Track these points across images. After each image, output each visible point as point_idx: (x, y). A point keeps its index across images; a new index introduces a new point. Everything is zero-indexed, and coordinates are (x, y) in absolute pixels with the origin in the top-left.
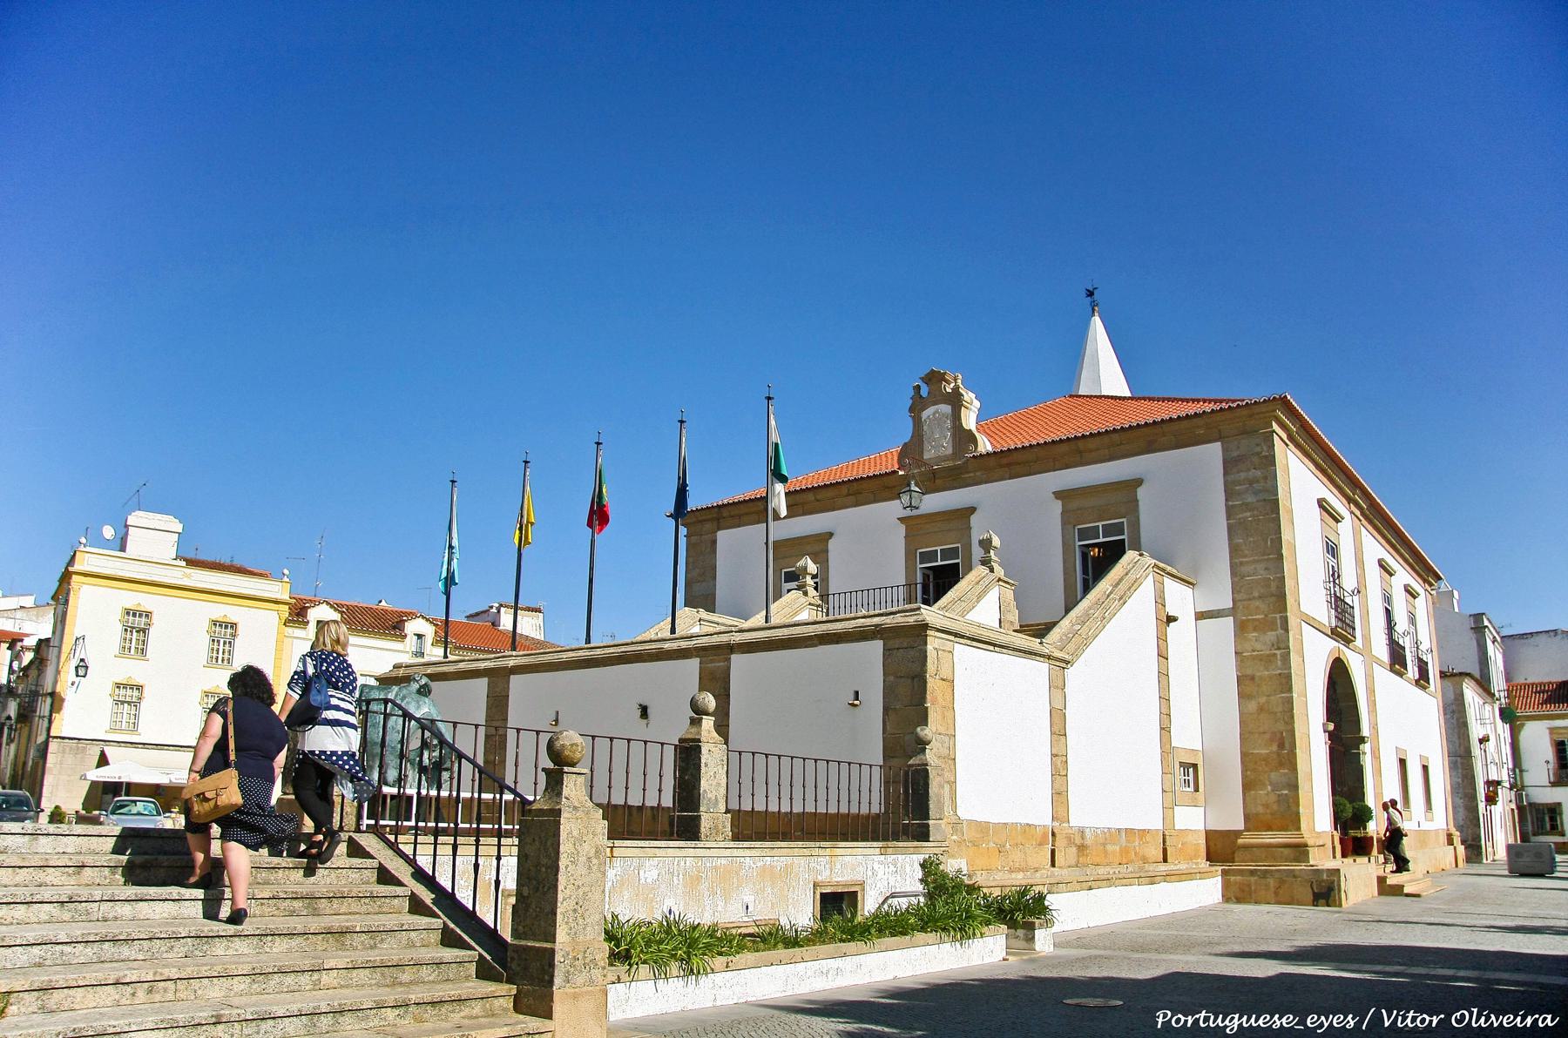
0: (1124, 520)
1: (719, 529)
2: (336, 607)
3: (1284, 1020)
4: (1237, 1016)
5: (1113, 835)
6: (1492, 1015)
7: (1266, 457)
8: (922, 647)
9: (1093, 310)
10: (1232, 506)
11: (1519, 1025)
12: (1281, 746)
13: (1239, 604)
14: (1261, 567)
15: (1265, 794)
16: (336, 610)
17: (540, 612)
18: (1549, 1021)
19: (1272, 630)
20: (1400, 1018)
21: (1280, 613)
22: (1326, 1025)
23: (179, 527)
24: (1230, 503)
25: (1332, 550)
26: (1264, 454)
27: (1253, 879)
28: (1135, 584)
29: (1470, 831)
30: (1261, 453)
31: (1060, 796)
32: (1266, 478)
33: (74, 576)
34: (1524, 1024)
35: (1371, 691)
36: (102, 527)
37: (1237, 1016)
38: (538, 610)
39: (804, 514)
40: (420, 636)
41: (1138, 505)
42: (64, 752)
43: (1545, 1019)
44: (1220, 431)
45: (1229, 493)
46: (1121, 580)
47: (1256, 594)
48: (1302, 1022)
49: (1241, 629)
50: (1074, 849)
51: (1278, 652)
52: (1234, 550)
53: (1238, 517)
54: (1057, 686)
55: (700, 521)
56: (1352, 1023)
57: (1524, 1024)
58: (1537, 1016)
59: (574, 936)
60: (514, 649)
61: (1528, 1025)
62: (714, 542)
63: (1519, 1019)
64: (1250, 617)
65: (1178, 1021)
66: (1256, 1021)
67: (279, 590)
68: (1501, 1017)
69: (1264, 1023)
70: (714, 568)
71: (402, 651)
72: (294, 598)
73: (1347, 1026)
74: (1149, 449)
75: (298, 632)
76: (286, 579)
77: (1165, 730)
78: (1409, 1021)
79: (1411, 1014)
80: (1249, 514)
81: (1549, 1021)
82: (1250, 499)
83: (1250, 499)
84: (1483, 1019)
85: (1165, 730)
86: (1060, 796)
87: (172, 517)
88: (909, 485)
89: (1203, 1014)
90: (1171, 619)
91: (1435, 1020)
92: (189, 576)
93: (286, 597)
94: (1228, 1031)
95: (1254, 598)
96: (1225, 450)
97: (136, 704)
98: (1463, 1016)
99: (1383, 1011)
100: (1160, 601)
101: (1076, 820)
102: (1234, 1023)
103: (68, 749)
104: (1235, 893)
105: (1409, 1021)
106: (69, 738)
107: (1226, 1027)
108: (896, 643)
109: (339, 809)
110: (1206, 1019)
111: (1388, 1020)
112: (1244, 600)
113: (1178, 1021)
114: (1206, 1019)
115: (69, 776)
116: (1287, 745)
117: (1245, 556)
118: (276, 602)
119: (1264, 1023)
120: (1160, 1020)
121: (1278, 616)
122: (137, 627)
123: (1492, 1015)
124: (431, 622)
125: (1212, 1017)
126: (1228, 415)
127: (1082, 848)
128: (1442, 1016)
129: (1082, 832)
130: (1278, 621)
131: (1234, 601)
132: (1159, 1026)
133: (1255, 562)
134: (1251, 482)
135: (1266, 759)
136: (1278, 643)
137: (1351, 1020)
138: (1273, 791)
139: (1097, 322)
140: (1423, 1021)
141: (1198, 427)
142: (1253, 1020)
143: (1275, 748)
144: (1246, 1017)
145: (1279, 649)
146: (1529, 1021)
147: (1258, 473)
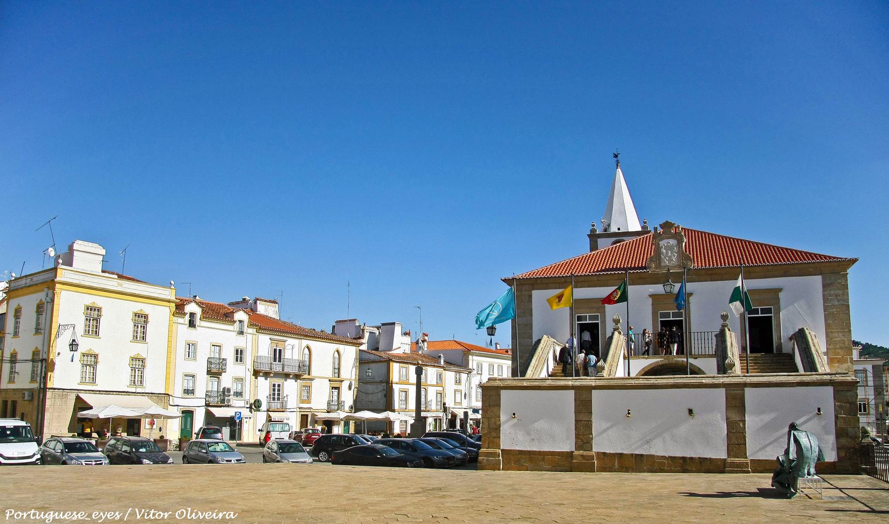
0: (772, 307)
1: (534, 289)
2: (199, 304)
3: (79, 515)
4: (52, 513)
6: (199, 512)
7: (843, 285)
8: (855, 391)
9: (617, 165)
11: (215, 518)
14: (840, 334)
16: (199, 306)
17: (277, 303)
18: (232, 515)
19: (845, 363)
20: (146, 514)
21: (850, 356)
22: (103, 518)
23: (103, 252)
24: (826, 304)
32: (843, 294)
34: (217, 517)
36: (588, 331)
37: (52, 513)
38: (275, 302)
39: (589, 287)
41: (779, 301)
43: (230, 514)
44: (821, 271)
45: (825, 300)
48: (90, 516)
52: (827, 326)
55: (522, 284)
56: (118, 517)
57: (217, 517)
58: (225, 513)
61: (220, 518)
62: (530, 296)
63: (215, 514)
65: (18, 515)
66: (44, 516)
67: (169, 294)
68: (204, 513)
69: (68, 517)
71: (232, 331)
72: (179, 299)
73: (116, 519)
74: (785, 274)
75: (181, 320)
78: (151, 515)
79: (152, 511)
80: (835, 310)
81: (232, 515)
82: (836, 303)
83: (836, 303)
84: (194, 514)
87: (98, 245)
88: (668, 281)
89: (33, 511)
91: (166, 515)
92: (121, 285)
93: (173, 298)
94: (47, 521)
95: (837, 348)
96: (823, 280)
98: (182, 513)
99: (137, 510)
102: (50, 516)
105: (151, 515)
107: (46, 519)
108: (841, 388)
110: (34, 515)
111: (202, 516)
113: (18, 515)
114: (34, 515)
118: (169, 301)
119: (68, 517)
120: (8, 515)
122: (93, 316)
123: (199, 512)
124: (247, 313)
125: (38, 513)
126: (827, 264)
128: (171, 513)
130: (849, 359)
132: (7, 518)
133: (837, 332)
134: (836, 296)
136: (848, 369)
137: (118, 515)
139: (619, 172)
140: (159, 515)
142: (61, 515)
144: (57, 513)
146: (220, 515)
147: (840, 292)
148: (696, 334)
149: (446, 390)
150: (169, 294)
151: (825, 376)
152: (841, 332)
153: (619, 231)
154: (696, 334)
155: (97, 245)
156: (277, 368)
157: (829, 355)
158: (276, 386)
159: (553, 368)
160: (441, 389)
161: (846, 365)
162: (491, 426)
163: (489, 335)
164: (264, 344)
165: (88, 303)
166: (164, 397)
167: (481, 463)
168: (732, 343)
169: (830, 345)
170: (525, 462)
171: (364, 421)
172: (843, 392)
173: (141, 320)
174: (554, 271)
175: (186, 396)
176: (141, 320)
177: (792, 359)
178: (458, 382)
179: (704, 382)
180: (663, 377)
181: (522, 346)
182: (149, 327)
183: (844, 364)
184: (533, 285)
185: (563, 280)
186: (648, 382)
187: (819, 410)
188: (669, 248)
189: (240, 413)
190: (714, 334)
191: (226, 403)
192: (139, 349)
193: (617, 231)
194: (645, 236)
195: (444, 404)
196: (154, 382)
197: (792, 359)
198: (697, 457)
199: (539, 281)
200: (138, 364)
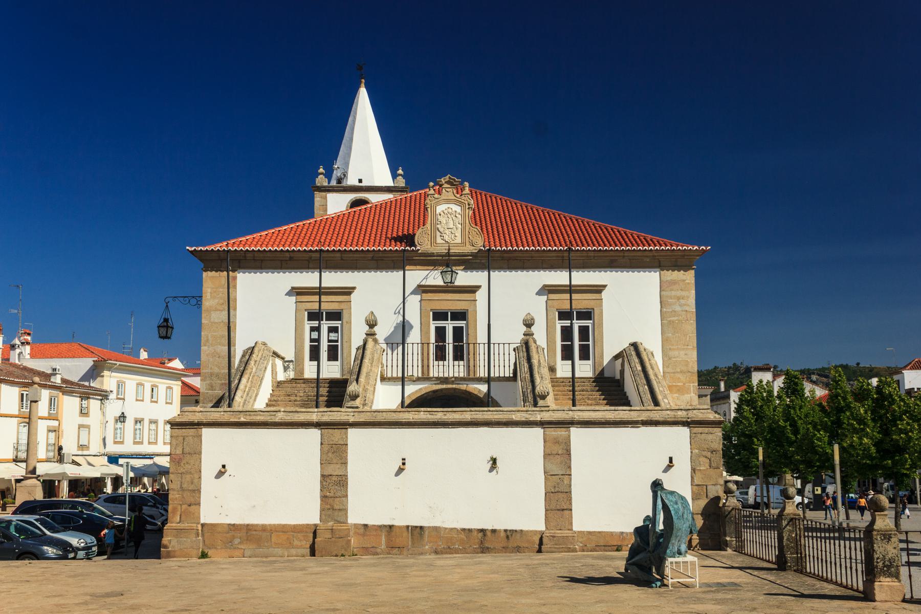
10: (666, 311)
13: (667, 375)
19: (687, 393)
26: (687, 281)
30: (685, 280)
47: (679, 370)
53: (669, 319)
60: (317, 407)
64: (674, 384)
109: (825, 572)
112: (671, 373)
115: (739, 604)
117: (673, 345)
121: (692, 385)
130: (692, 389)
136: (691, 402)
139: (363, 97)
141: (647, 257)
148: (496, 346)
149: (64, 427)
151: (680, 413)
153: (360, 184)
154: (496, 346)
158: (24, 407)
159: (271, 392)
160: (55, 423)
161: (689, 395)
162: (185, 486)
163: (161, 337)
167: (166, 547)
168: (539, 361)
169: (668, 367)
170: (240, 543)
171: (86, 479)
172: (703, 435)
174: (320, 233)
177: (619, 386)
178: (84, 413)
179: (514, 417)
180: (455, 409)
181: (219, 357)
183: (686, 395)
184: (239, 262)
185: (287, 255)
186: (432, 417)
187: (494, 461)
188: (447, 214)
190: (512, 346)
193: (357, 184)
194: (424, 191)
195: (60, 448)
197: (619, 386)
198: (619, 531)
199: (249, 255)
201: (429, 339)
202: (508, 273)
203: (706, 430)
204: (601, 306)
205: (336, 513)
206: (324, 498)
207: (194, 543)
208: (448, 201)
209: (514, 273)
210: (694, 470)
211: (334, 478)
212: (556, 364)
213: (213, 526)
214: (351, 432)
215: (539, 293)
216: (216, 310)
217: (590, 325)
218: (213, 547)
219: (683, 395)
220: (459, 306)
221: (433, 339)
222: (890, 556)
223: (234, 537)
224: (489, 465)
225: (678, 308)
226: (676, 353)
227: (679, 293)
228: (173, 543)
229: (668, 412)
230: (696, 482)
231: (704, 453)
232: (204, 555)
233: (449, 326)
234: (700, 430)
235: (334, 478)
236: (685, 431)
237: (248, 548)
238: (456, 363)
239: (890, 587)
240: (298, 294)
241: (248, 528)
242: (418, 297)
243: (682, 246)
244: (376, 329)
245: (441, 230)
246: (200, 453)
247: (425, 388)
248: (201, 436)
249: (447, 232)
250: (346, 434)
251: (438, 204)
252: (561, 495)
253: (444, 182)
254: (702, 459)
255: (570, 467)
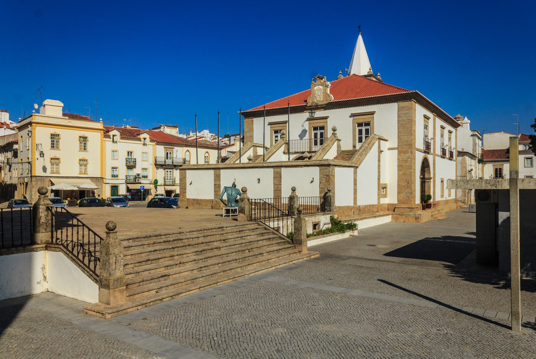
5: (366, 207)
12: (408, 183)
15: (403, 195)
23: (62, 105)
25: (426, 127)
27: (399, 216)
28: (374, 144)
29: (463, 198)
31: (355, 199)
33: (33, 124)
35: (434, 164)
40: (145, 139)
42: (37, 181)
46: (370, 143)
47: (404, 144)
49: (400, 153)
50: (358, 211)
51: (409, 159)
54: (355, 173)
59: (303, 237)
70: (253, 128)
76: (101, 122)
77: (379, 179)
85: (379, 179)
86: (355, 199)
90: (381, 151)
92: (70, 122)
93: (102, 128)
97: (58, 164)
100: (379, 147)
101: (358, 204)
103: (38, 180)
104: (395, 219)
106: (39, 176)
116: (409, 183)
127: (360, 210)
129: (359, 206)
131: (398, 145)
135: (404, 186)
138: (405, 194)
139: (360, 39)
143: (406, 183)
145: (409, 158)
150: (99, 125)
152: (406, 135)
155: (58, 101)
156: (169, 162)
157: (399, 149)
164: (161, 151)
165: (52, 132)
166: (99, 180)
169: (400, 143)
173: (84, 140)
175: (113, 178)
176: (84, 140)
182: (88, 143)
187: (259, 180)
189: (144, 186)
191: (137, 182)
192: (83, 155)
196: (93, 170)
200: (83, 162)
201: (311, 137)
202: (340, 110)
203: (325, 168)
204: (373, 120)
205: (218, 196)
206: (215, 191)
207: (185, 204)
208: (318, 85)
209: (342, 109)
210: (320, 183)
211: (217, 185)
212: (356, 144)
213: (189, 199)
214: (222, 171)
215: (350, 117)
216: (248, 132)
217: (369, 128)
218: (189, 205)
219: (406, 154)
220: (321, 125)
221: (313, 137)
222: (243, 206)
223: (194, 203)
224: (258, 181)
225: (405, 118)
226: (403, 137)
227: (406, 112)
228: (180, 204)
229: (314, 162)
230: (321, 187)
231: (324, 176)
232: (187, 208)
233: (319, 132)
234: (323, 168)
235: (217, 185)
236: (318, 169)
237: (197, 206)
238: (315, 146)
239: (242, 217)
240: (271, 124)
241: (197, 200)
242: (308, 122)
243: (410, 91)
244: (336, 132)
245: (316, 96)
246: (186, 178)
247: (298, 156)
248: (186, 173)
249: (318, 97)
250: (220, 171)
251: (315, 86)
252: (278, 191)
253: (316, 78)
254: (324, 179)
255: (281, 182)
